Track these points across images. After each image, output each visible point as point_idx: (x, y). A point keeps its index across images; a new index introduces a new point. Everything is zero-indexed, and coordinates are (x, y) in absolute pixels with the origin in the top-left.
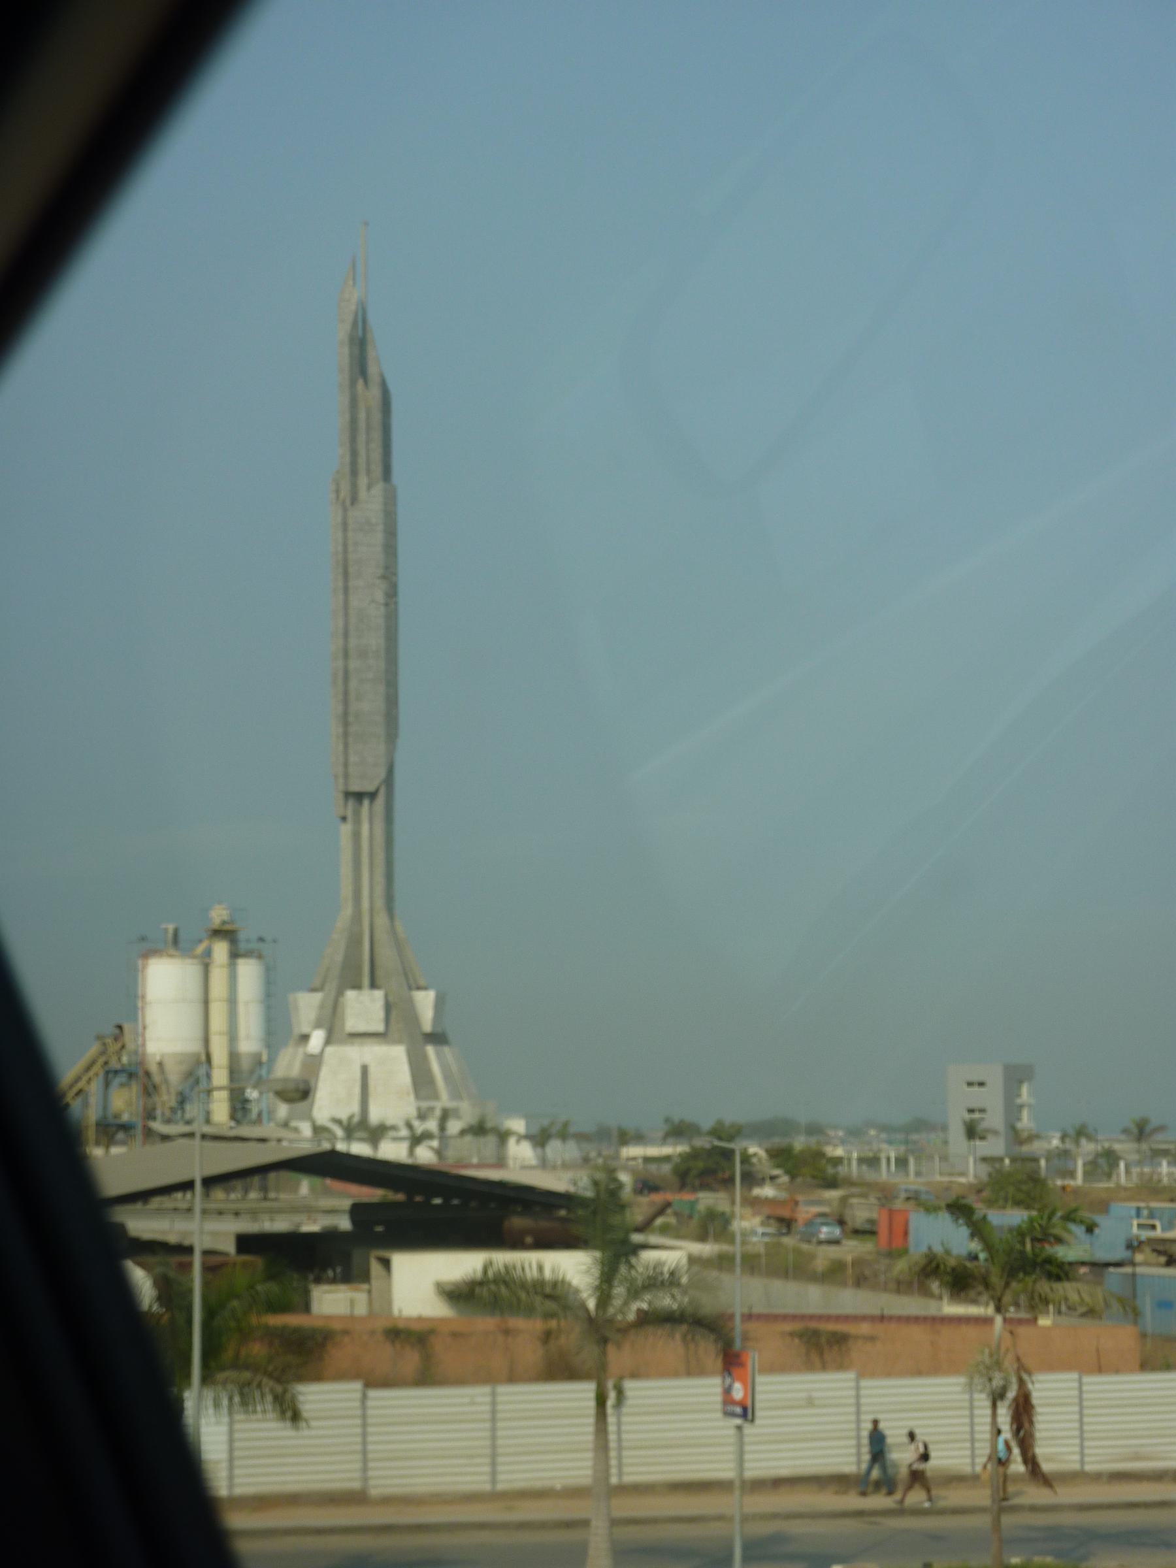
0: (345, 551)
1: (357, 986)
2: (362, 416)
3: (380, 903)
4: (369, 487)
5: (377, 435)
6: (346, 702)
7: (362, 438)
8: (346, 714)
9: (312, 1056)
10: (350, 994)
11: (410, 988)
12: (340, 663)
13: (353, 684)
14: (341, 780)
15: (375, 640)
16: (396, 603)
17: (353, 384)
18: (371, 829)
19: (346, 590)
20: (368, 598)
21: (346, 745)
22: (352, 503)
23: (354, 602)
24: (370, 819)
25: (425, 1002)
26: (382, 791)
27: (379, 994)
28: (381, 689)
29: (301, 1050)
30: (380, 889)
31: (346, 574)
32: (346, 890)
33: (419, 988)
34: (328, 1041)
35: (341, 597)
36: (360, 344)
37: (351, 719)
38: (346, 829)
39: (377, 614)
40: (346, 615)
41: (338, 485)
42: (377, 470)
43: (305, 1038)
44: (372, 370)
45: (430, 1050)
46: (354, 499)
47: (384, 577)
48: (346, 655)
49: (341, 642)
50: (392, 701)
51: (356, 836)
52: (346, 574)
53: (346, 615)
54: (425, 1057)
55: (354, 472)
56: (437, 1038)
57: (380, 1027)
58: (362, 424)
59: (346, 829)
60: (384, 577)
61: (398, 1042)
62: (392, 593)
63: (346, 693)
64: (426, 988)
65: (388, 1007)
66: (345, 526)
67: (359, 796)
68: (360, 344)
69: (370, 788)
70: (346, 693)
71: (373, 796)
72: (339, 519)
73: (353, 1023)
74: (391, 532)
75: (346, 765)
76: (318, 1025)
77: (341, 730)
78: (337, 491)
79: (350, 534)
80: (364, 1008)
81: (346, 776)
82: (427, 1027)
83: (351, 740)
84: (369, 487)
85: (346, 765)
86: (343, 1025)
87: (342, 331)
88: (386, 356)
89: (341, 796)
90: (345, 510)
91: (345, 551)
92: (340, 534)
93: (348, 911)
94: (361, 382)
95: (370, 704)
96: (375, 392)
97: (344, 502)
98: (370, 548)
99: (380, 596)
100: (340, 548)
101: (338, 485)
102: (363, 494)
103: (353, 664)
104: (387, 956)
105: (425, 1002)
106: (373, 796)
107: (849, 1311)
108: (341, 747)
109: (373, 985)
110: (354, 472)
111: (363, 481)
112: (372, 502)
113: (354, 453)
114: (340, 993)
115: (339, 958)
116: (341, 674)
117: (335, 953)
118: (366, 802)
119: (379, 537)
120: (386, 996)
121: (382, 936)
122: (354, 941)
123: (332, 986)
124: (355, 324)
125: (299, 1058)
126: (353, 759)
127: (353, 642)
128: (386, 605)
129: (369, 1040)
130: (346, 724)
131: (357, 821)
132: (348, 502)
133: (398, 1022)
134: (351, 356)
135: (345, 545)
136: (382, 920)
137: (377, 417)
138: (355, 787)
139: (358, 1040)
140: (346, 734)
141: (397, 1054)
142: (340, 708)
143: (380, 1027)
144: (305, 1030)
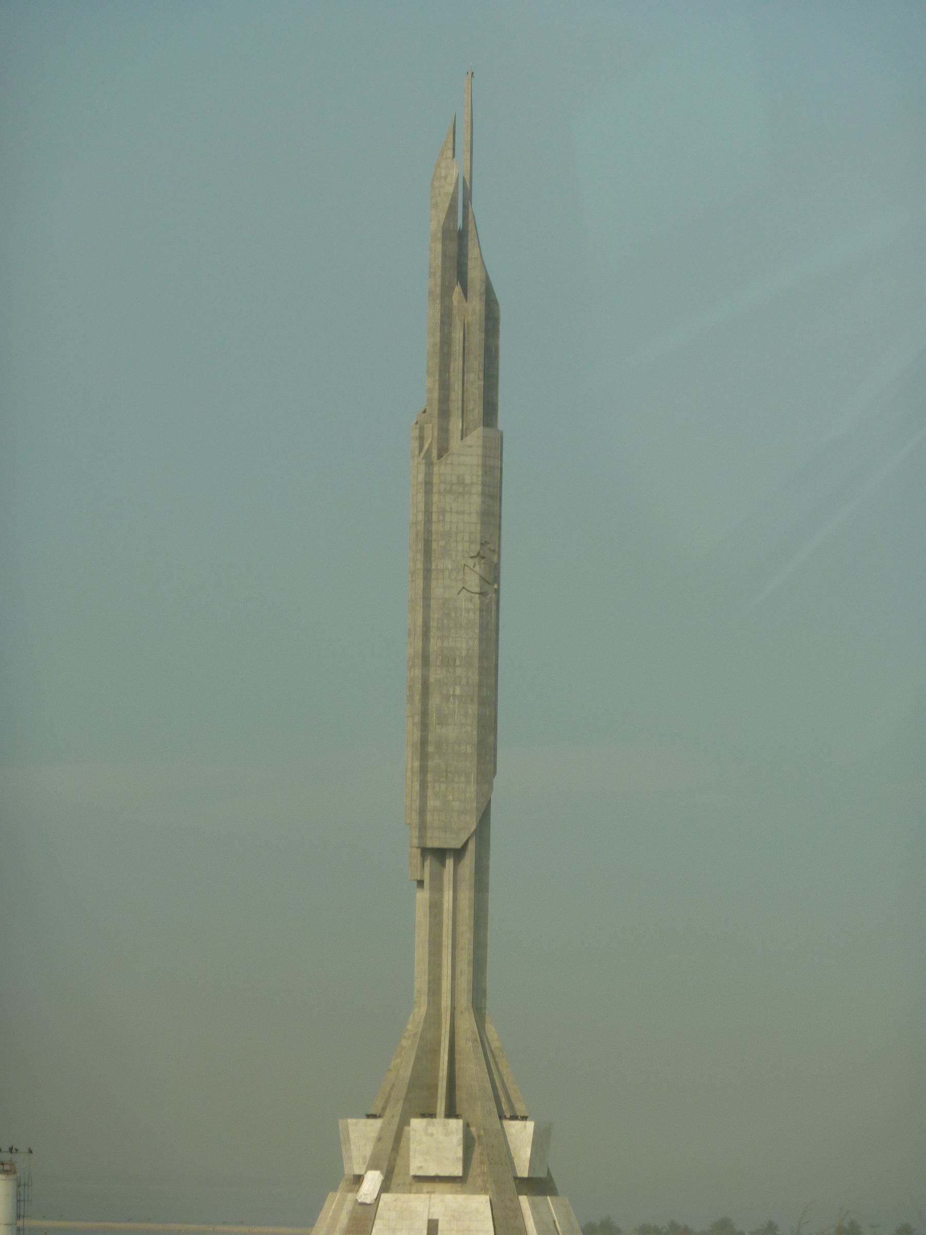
0: (428, 521)
1: (429, 1114)
2: (458, 335)
3: (464, 1000)
4: (463, 435)
5: (476, 362)
6: (424, 726)
7: (456, 364)
8: (424, 742)
9: (363, 1204)
10: (417, 1124)
11: (502, 1117)
12: (418, 672)
13: (435, 701)
14: (416, 833)
15: (465, 643)
16: (497, 591)
17: (446, 293)
18: (455, 899)
19: (427, 573)
20: (458, 586)
21: (423, 784)
22: (440, 456)
23: (437, 591)
24: (455, 881)
25: (521, 1136)
26: (472, 847)
27: (456, 1125)
28: (473, 709)
29: (350, 1196)
30: (464, 982)
31: (428, 552)
32: (421, 982)
33: (514, 1118)
34: (385, 1187)
35: (420, 583)
36: (457, 241)
37: (431, 749)
38: (423, 896)
39: (468, 607)
40: (427, 607)
41: (422, 429)
42: (476, 409)
43: (358, 1180)
44: (474, 274)
45: (524, 1201)
46: (443, 450)
47: (479, 556)
48: (426, 661)
49: (419, 644)
50: (488, 725)
51: (435, 907)
52: (428, 552)
53: (427, 607)
54: (517, 1211)
55: (444, 414)
56: (539, 1185)
57: (458, 1171)
58: (457, 347)
59: (423, 896)
60: (479, 556)
61: (483, 1190)
62: (492, 577)
63: (425, 714)
64: (524, 1118)
65: (468, 1144)
66: (428, 485)
67: (440, 854)
68: (457, 241)
69: (457, 844)
70: (425, 714)
71: (458, 854)
72: (421, 477)
73: (418, 1164)
74: (492, 494)
75: (422, 811)
76: (373, 1165)
77: (417, 764)
78: (421, 439)
79: (435, 498)
80: (436, 1143)
81: (423, 827)
82: (523, 1171)
83: (430, 777)
84: (463, 435)
85: (422, 811)
86: (407, 1167)
87: (435, 221)
88: (492, 253)
89: (418, 852)
90: (429, 464)
91: (428, 521)
92: (421, 498)
93: (421, 1010)
94: (458, 289)
95: (458, 729)
96: (476, 304)
97: (429, 451)
98: (462, 517)
99: (473, 582)
100: (421, 517)
101: (422, 429)
102: (455, 443)
103: (434, 675)
104: (471, 1071)
105: (521, 1136)
106: (458, 854)
107: (462, 334)
108: (417, 786)
109: (451, 1113)
110: (444, 414)
111: (456, 424)
112: (467, 453)
113: (445, 386)
114: (404, 1122)
115: (406, 1073)
116: (418, 686)
117: (403, 1067)
118: (450, 863)
119: (475, 501)
120: (467, 1126)
121: (465, 1044)
122: (427, 1052)
123: (395, 1111)
124: (452, 211)
125: (348, 1206)
126: (432, 803)
127: (435, 644)
128: (482, 594)
129: (440, 1186)
130: (424, 756)
131: (437, 889)
132: (435, 452)
133: (482, 1159)
134: (444, 254)
135: (428, 513)
136: (466, 1023)
137: (477, 338)
138: (434, 842)
139: (426, 1187)
140: (423, 770)
141: (478, 1207)
142: (417, 734)
143: (458, 1171)
144: (357, 1171)
